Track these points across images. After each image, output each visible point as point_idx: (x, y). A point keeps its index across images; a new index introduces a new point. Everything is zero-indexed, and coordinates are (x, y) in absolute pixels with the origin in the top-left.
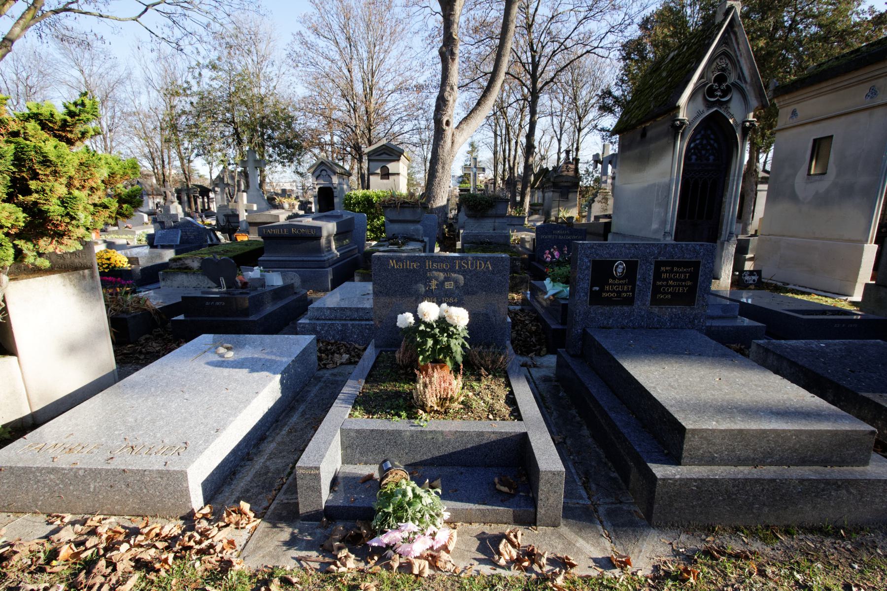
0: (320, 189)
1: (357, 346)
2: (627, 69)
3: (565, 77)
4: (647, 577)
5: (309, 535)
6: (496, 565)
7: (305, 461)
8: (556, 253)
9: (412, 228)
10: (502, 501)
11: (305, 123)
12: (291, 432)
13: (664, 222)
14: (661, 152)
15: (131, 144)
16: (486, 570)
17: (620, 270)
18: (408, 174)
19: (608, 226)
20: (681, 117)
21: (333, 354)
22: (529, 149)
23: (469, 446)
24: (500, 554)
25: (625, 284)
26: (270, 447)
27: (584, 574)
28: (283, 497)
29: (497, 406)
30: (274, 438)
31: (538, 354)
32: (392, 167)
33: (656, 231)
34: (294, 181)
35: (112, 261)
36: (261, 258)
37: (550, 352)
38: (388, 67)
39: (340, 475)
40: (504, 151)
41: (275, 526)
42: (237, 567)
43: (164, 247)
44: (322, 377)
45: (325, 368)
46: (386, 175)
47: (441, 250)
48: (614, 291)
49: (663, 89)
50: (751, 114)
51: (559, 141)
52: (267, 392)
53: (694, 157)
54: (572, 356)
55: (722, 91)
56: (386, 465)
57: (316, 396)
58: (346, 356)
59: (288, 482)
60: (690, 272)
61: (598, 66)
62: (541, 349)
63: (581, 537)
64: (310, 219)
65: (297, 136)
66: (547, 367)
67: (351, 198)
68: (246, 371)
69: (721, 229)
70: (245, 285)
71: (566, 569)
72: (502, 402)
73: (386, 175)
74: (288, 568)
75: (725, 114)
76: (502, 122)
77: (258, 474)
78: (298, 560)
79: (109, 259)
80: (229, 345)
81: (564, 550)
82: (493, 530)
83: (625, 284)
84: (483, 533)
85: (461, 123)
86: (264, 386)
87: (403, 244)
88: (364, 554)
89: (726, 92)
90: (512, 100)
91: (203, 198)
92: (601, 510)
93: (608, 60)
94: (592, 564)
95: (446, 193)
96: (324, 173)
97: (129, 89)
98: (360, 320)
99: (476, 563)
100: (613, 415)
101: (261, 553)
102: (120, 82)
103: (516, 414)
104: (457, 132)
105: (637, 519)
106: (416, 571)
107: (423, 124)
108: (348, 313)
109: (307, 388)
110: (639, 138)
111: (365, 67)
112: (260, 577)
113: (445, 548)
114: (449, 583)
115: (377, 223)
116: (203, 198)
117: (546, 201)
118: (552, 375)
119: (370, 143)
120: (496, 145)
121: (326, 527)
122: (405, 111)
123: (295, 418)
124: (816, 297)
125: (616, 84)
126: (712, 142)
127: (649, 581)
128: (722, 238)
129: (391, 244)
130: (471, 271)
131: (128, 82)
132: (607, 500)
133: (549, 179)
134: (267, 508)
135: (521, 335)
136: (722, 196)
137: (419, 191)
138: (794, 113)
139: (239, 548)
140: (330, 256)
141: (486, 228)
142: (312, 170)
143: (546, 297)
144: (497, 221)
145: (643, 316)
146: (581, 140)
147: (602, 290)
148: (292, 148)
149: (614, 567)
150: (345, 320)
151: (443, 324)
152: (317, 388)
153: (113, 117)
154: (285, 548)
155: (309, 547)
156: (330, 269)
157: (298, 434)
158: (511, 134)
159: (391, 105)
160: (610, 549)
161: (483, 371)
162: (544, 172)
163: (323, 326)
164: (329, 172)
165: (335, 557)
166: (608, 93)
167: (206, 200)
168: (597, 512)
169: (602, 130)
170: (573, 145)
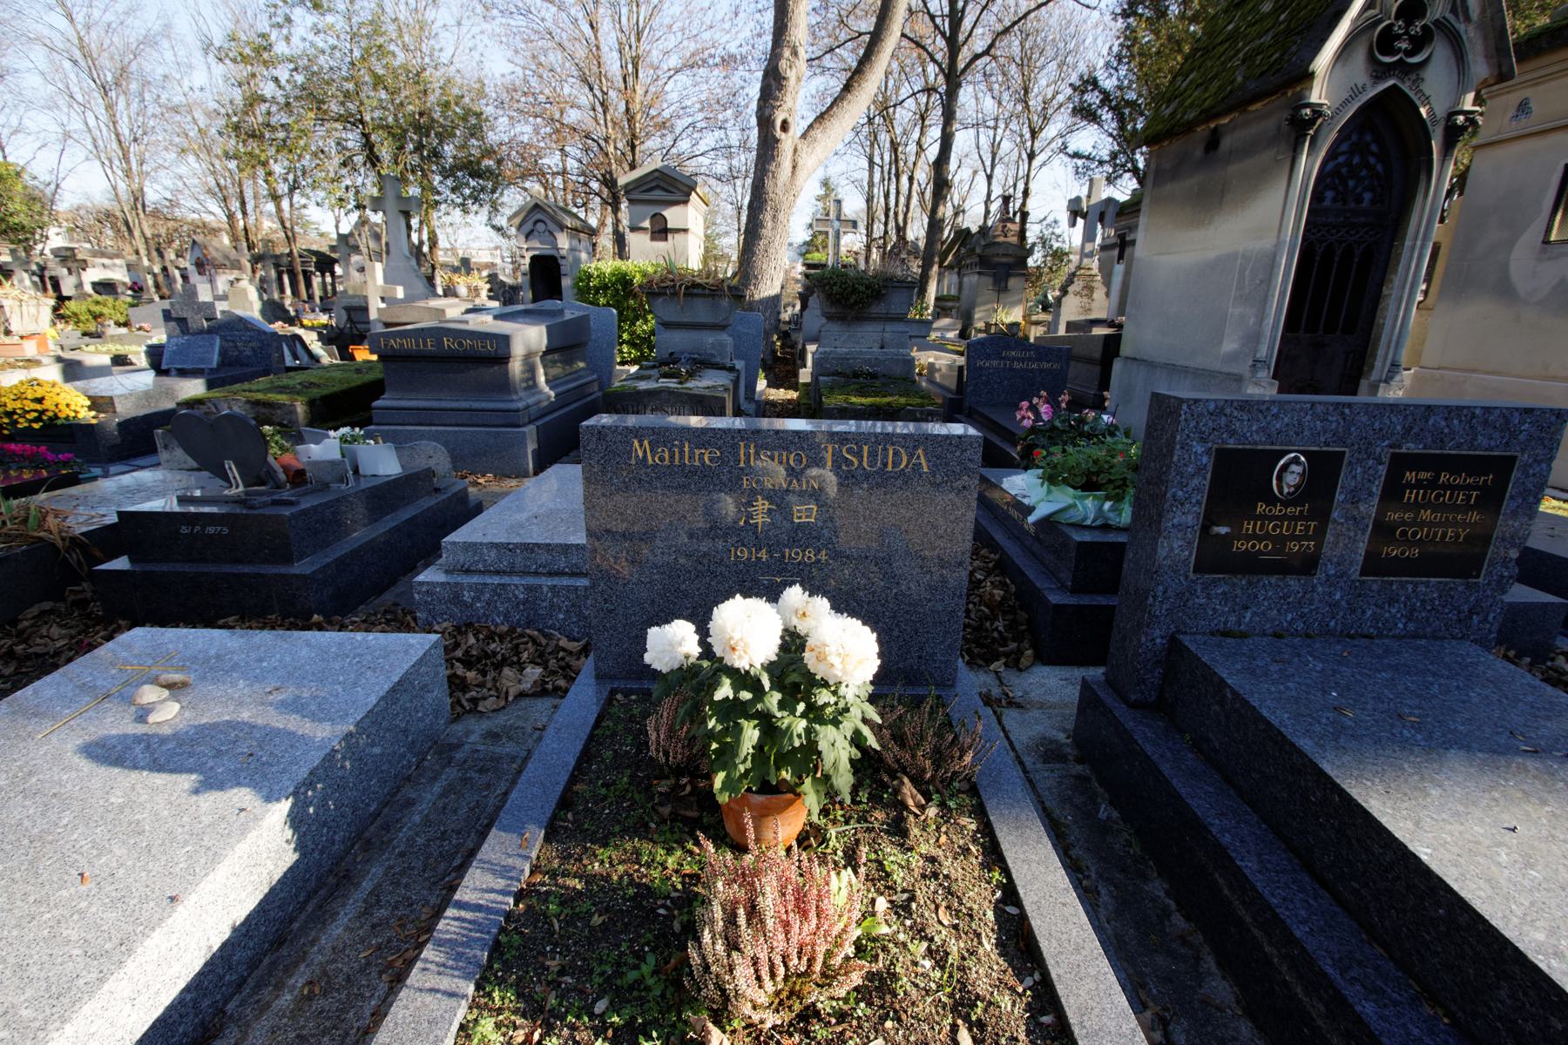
0: (533, 258)
1: (564, 642)
2: (1130, 37)
3: (1013, 45)
8: (1044, 409)
9: (711, 340)
11: (503, 130)
12: (310, 998)
13: (1254, 338)
14: (1256, 182)
15: (183, 170)
17: (1292, 479)
18: (707, 236)
19: (1112, 345)
20: (1314, 97)
21: (498, 667)
22: (941, 185)
25: (1301, 517)
31: (1014, 663)
32: (673, 215)
33: (1233, 357)
34: (496, 248)
35: (48, 404)
36: (376, 403)
38: (667, 21)
40: (887, 196)
43: (183, 373)
44: (459, 746)
45: (474, 711)
46: (661, 231)
47: (769, 386)
48: (1267, 536)
49: (1267, 38)
50: (1470, 96)
51: (989, 178)
52: (248, 853)
53: (1329, 194)
54: (1133, 706)
55: (1412, 39)
57: (427, 822)
58: (533, 673)
60: (1483, 488)
61: (1072, 29)
64: (490, 318)
65: (489, 152)
66: (1042, 706)
67: (590, 276)
69: (1374, 356)
70: (298, 477)
72: (988, 946)
73: (661, 231)
75: (1411, 94)
76: (884, 138)
79: (40, 400)
80: (177, 677)
83: (1301, 517)
85: (811, 126)
86: (215, 859)
87: (691, 375)
89: (1419, 43)
90: (905, 91)
91: (323, 276)
93: (1096, 14)
95: (779, 275)
96: (540, 227)
97: (168, 55)
98: (573, 575)
102: (149, 41)
104: (802, 146)
107: (735, 137)
108: (544, 557)
109: (409, 792)
110: (1199, 153)
111: (624, 20)
115: (642, 327)
116: (323, 276)
117: (965, 292)
118: (1061, 737)
119: (633, 167)
120: (871, 184)
122: (701, 110)
124: (1555, 503)
125: (1107, 65)
126: (1372, 160)
128: (1374, 376)
129: (665, 376)
130: (867, 476)
131: (165, 44)
133: (973, 250)
136: (1382, 281)
137: (728, 270)
138: (1523, 107)
140: (531, 401)
141: (864, 342)
142: (517, 221)
143: (1031, 519)
144: (889, 328)
145: (1336, 604)
146: (1033, 173)
148: (479, 175)
150: (536, 573)
151: (793, 669)
152: (437, 788)
153: (142, 112)
158: (901, 164)
159: (674, 97)
161: (909, 793)
162: (963, 235)
163: (479, 589)
164: (551, 226)
166: (1091, 83)
167: (329, 279)
169: (1076, 155)
170: (1015, 186)
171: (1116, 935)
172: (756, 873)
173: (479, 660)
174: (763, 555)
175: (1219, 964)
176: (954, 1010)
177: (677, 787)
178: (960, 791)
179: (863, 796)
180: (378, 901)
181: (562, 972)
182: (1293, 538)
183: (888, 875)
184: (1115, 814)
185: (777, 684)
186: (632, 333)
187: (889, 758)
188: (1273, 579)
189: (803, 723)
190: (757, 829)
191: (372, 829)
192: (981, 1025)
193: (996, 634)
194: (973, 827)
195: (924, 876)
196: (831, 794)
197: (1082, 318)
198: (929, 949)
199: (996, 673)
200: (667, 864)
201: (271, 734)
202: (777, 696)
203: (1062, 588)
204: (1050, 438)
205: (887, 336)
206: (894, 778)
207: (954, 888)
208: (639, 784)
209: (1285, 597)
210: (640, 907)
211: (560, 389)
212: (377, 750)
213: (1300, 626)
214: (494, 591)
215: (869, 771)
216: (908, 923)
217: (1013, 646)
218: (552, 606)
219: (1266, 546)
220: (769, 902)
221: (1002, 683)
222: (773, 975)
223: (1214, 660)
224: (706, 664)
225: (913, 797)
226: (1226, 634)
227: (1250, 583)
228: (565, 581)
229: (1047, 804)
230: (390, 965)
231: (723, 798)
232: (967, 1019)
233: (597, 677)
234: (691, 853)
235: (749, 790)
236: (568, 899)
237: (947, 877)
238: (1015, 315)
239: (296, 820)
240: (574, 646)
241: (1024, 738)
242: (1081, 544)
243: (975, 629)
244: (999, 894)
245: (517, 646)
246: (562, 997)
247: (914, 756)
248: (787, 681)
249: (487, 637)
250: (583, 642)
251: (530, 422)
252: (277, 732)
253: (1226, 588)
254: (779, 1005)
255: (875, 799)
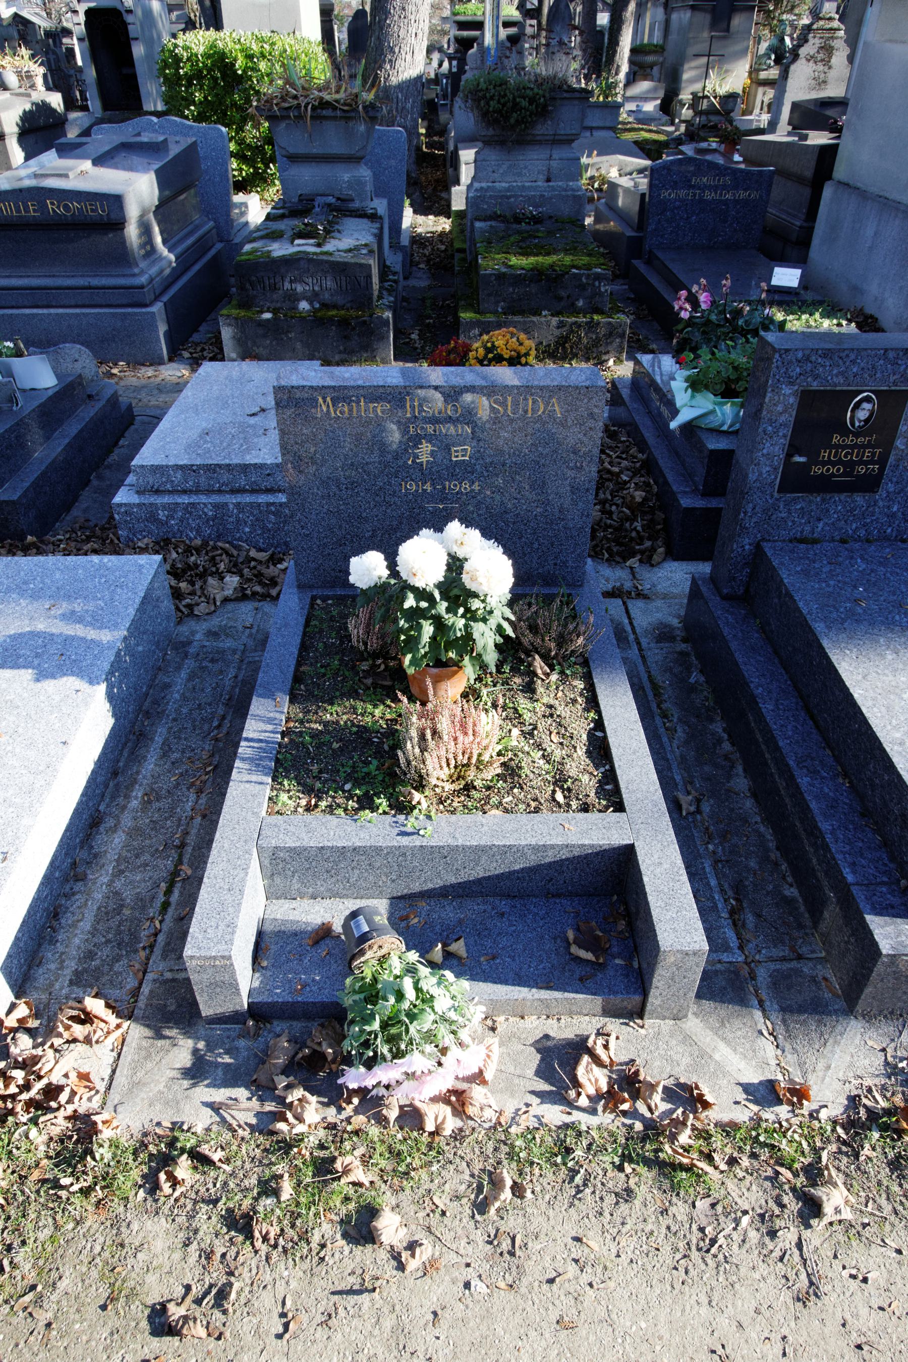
0: (88, 12)
1: (253, 553)
4: (835, 1122)
5: (227, 1052)
6: (571, 1105)
7: (195, 948)
8: (703, 297)
9: (346, 177)
10: (581, 979)
12: (149, 802)
16: (554, 1114)
17: (862, 415)
21: (203, 576)
23: (517, 867)
24: (577, 1084)
25: (869, 445)
26: (113, 844)
27: (725, 1117)
28: (162, 966)
29: (572, 769)
30: (117, 818)
31: (648, 560)
37: (676, 554)
39: (268, 928)
41: (159, 1036)
42: (106, 1133)
44: (190, 643)
45: (191, 614)
54: (725, 598)
56: (358, 926)
57: (184, 698)
58: (232, 581)
59: (165, 927)
62: (653, 550)
63: (724, 1039)
66: (665, 597)
67: (177, 59)
68: (27, 674)
71: (695, 1112)
72: (581, 752)
74: (199, 1129)
77: (103, 915)
78: (215, 1107)
81: (695, 1067)
82: (564, 1029)
83: (869, 445)
84: (547, 1037)
88: (334, 1095)
92: (762, 973)
94: (741, 1096)
98: (253, 491)
99: (535, 1101)
100: (804, 781)
101: (144, 1095)
103: (612, 797)
105: (827, 995)
106: (430, 1126)
108: (226, 477)
109: (162, 678)
112: (152, 1149)
113: (478, 1078)
114: (490, 1146)
118: (675, 622)
121: (257, 1035)
123: (150, 765)
127: (840, 1130)
129: (301, 235)
130: (512, 421)
132: (776, 952)
134: (135, 993)
135: (610, 513)
139: (101, 1086)
140: (153, 271)
145: (894, 515)
147: (814, 459)
149: (779, 1102)
150: (220, 491)
152: (184, 674)
154: (186, 1083)
155: (231, 1078)
156: (157, 308)
157: (164, 804)
160: (773, 1062)
161: (539, 665)
163: (172, 508)
165: (281, 1101)
168: (753, 978)
171: (681, 756)
172: (435, 712)
173: (184, 571)
174: (428, 487)
175: (745, 770)
176: (555, 784)
177: (374, 666)
178: (575, 663)
179: (507, 668)
180: (170, 749)
181: (320, 772)
182: (861, 462)
183: (520, 716)
184: (702, 679)
185: (445, 596)
186: (241, 142)
187: (525, 641)
188: (843, 496)
189: (463, 621)
190: (434, 689)
191: (146, 704)
192: (569, 790)
193: (634, 534)
194: (582, 686)
195: (544, 716)
196: (483, 667)
197: (814, 95)
198: (543, 756)
199: (631, 568)
200: (377, 714)
201: (68, 640)
202: (445, 604)
203: (695, 491)
204: (704, 333)
205: (554, 164)
206: (528, 655)
207: (563, 722)
208: (346, 665)
209: (852, 511)
210: (362, 738)
211: (179, 249)
212: (140, 648)
213: (862, 533)
214: (186, 509)
215: (512, 652)
216: (531, 742)
217: (648, 544)
218: (238, 521)
219: (838, 470)
220: (444, 725)
221: (634, 577)
222: (448, 765)
223: (782, 564)
224: (393, 581)
225: (541, 668)
226: (802, 541)
227: (823, 500)
228: (248, 499)
229: (653, 673)
230: (193, 784)
231: (411, 671)
232: (562, 788)
233: (299, 587)
234: (390, 707)
235: (428, 665)
236: (315, 735)
237: (559, 716)
238: (733, 78)
239: (110, 697)
240: (263, 556)
241: (645, 624)
242: (712, 451)
243: (616, 529)
244: (592, 725)
245: (213, 559)
246: (324, 783)
247: (543, 640)
248: (452, 594)
249: (185, 551)
250: (270, 552)
251: (157, 298)
252: (73, 638)
253: (803, 504)
254: (452, 780)
255: (515, 670)
